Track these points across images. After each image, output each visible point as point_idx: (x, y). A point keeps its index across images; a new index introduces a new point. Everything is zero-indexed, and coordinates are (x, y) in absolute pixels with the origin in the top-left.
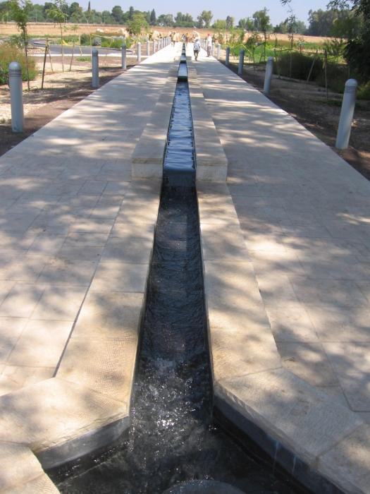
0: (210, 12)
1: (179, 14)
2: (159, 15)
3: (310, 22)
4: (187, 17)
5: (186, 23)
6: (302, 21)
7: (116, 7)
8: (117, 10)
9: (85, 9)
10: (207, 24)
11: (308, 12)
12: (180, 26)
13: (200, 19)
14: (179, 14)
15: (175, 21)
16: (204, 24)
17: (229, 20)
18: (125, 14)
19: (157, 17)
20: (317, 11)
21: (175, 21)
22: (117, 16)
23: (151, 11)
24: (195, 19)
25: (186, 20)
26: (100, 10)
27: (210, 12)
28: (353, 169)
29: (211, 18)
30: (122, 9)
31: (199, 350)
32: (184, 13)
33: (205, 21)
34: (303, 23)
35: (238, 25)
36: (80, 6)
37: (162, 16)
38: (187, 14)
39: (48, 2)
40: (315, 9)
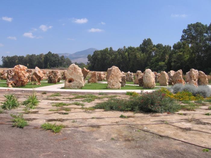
9: (169, 46)
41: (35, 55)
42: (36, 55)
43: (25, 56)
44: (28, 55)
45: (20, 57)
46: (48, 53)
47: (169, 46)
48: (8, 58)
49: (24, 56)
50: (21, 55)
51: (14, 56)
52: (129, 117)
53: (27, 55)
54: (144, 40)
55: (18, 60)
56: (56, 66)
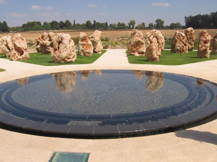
0: (134, 21)
1: (119, 23)
2: (110, 24)
3: (186, 23)
4: (123, 24)
5: (123, 27)
6: (179, 22)
7: (88, 21)
8: (88, 23)
9: (93, 23)
10: (133, 27)
11: (184, 17)
12: (119, 28)
13: (130, 25)
14: (119, 23)
15: (117, 27)
16: (131, 27)
17: (143, 24)
18: (163, 25)
19: (108, 25)
20: (189, 17)
21: (117, 27)
22: (88, 26)
23: (105, 22)
24: (127, 25)
25: (122, 26)
26: (81, 23)
27: (134, 21)
28: (166, 72)
29: (135, 23)
30: (91, 22)
31: (134, 71)
32: (121, 22)
33: (132, 25)
34: (180, 23)
35: (148, 26)
36: (70, 22)
37: (111, 25)
38: (123, 23)
39: (54, 21)
40: (188, 16)
41: (173, 23)
42: (193, 16)
43: (209, 15)
44: (213, 13)
45: (204, 16)
46: (12, 27)
47: (93, 23)
48: (191, 17)
49: (208, 15)
50: (205, 14)
51: (197, 16)
52: (24, 34)
53: (211, 13)
54: (133, 20)
55: (201, 20)
56: (113, 117)
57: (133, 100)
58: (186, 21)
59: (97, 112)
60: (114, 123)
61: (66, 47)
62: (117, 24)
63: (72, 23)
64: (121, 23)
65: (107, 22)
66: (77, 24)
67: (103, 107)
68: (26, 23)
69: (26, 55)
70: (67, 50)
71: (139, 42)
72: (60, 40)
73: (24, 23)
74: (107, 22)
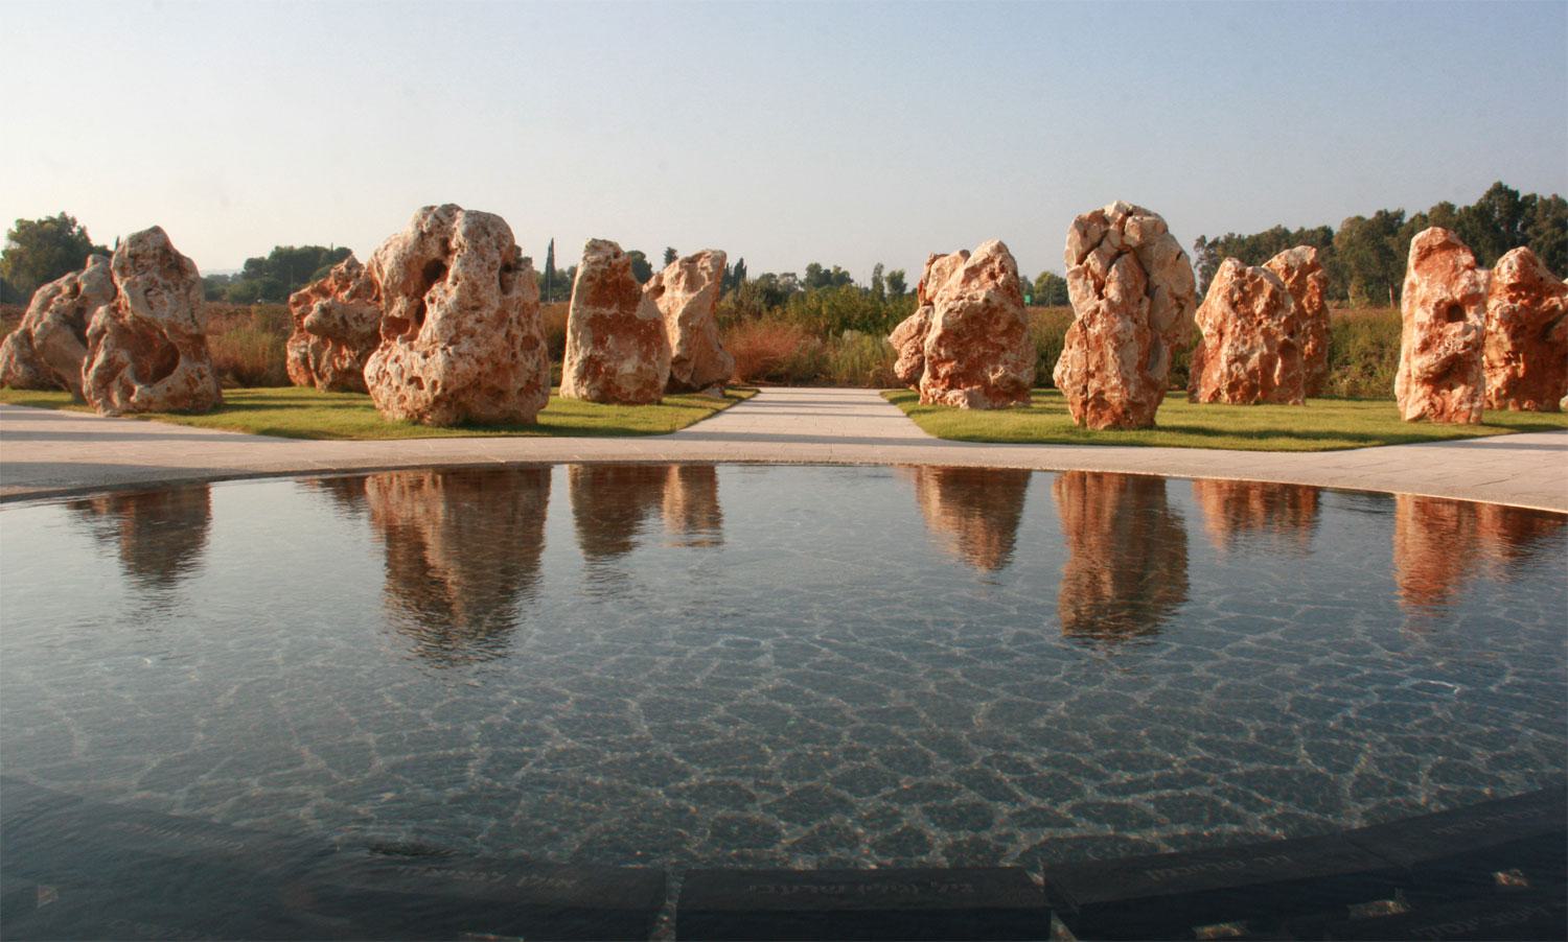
1: (814, 269)
14: (814, 269)
27: (277, 248)
57: (100, 664)
58: (1204, 263)
59: (789, 834)
60: (222, 436)
61: (475, 309)
62: (802, 275)
63: (539, 266)
64: (824, 267)
65: (742, 260)
66: (572, 258)
67: (850, 753)
68: (265, 253)
69: (195, 376)
70: (479, 328)
71: (990, 315)
72: (434, 251)
73: (256, 255)
74: (742, 260)
